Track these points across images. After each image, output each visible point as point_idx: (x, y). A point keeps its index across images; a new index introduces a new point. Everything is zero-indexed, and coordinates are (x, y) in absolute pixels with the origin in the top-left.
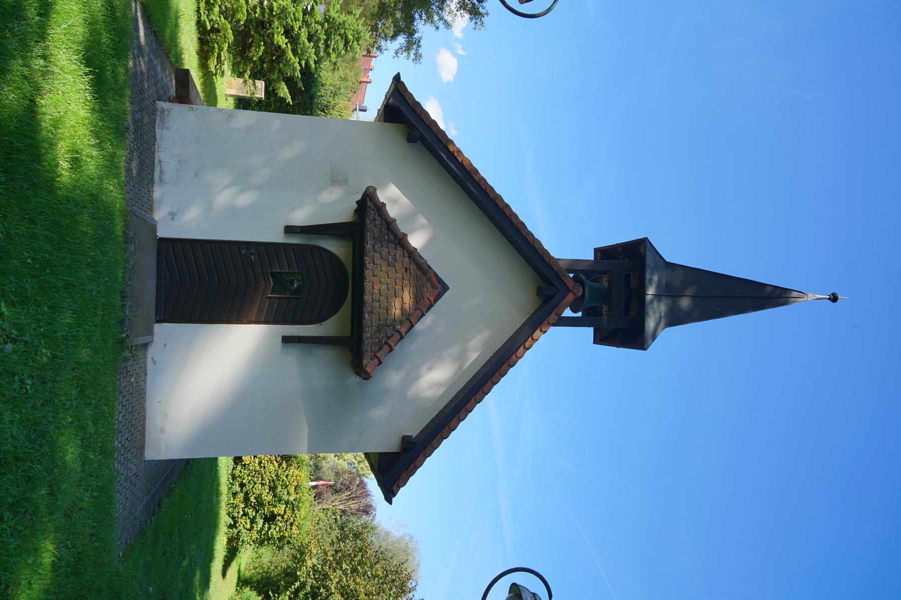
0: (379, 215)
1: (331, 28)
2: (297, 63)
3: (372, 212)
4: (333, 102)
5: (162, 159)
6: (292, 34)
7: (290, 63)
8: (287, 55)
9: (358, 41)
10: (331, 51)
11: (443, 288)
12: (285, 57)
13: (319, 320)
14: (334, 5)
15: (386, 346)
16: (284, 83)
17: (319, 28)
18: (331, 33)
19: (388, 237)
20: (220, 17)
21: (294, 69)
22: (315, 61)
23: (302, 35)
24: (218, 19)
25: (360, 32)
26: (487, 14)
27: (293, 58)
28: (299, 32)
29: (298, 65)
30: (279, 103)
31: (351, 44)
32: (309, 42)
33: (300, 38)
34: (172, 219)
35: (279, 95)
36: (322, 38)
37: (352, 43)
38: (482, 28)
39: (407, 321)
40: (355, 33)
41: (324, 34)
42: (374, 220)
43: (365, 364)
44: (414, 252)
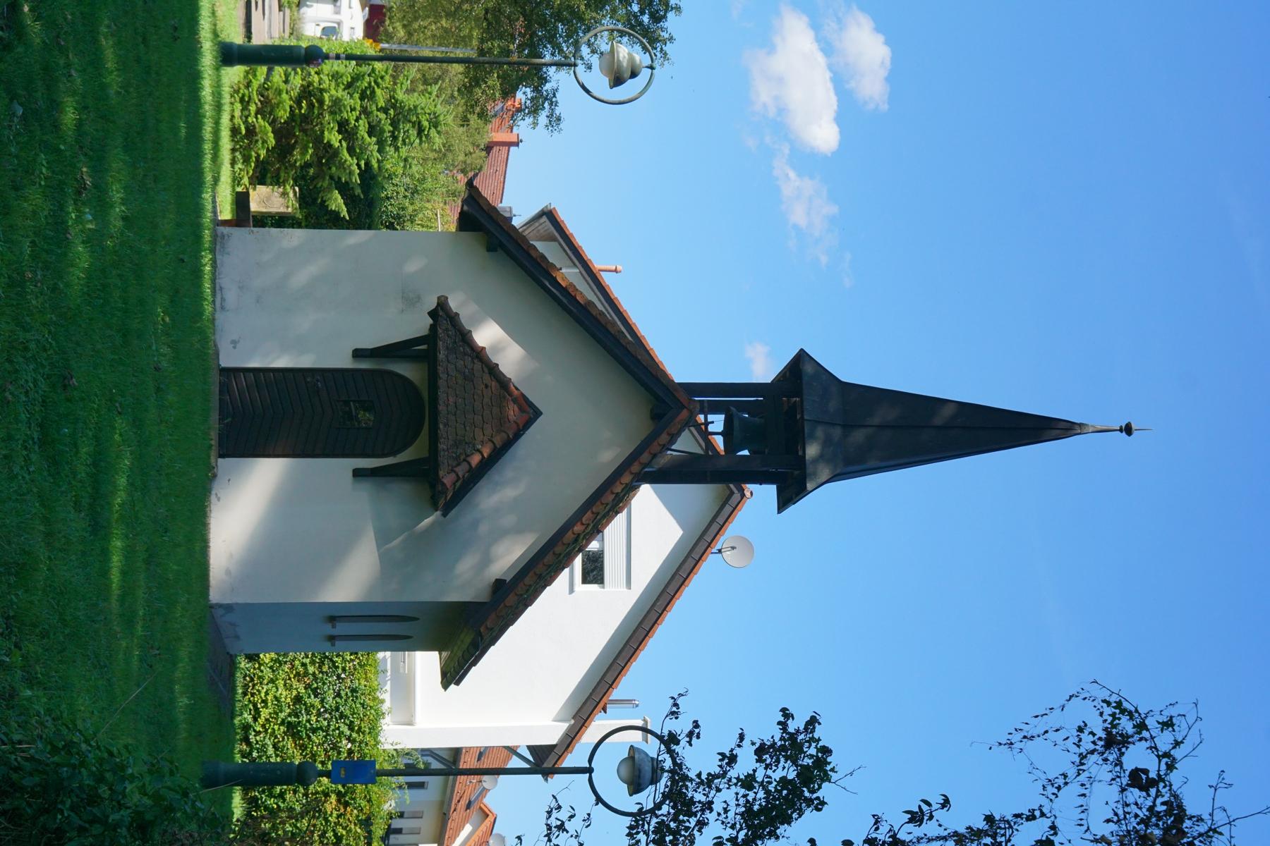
0: (453, 325)
1: (399, 114)
2: (355, 165)
3: (445, 322)
4: (411, 208)
5: (223, 286)
6: (347, 127)
7: (345, 166)
8: (341, 155)
9: (436, 127)
10: (399, 145)
11: (535, 414)
12: (339, 159)
13: (393, 453)
14: (402, 84)
15: (465, 463)
16: (337, 192)
17: (382, 116)
18: (399, 120)
19: (464, 349)
20: (257, 118)
21: (351, 173)
22: (378, 159)
23: (360, 128)
24: (254, 120)
25: (438, 116)
26: (671, 39)
27: (349, 159)
28: (357, 124)
29: (356, 167)
30: (314, 218)
31: (426, 133)
32: (370, 136)
33: (357, 133)
34: (235, 347)
35: (329, 209)
36: (387, 130)
37: (428, 132)
38: (667, 62)
39: (490, 442)
40: (432, 116)
41: (389, 124)
42: (447, 330)
43: (441, 476)
44: (494, 367)
